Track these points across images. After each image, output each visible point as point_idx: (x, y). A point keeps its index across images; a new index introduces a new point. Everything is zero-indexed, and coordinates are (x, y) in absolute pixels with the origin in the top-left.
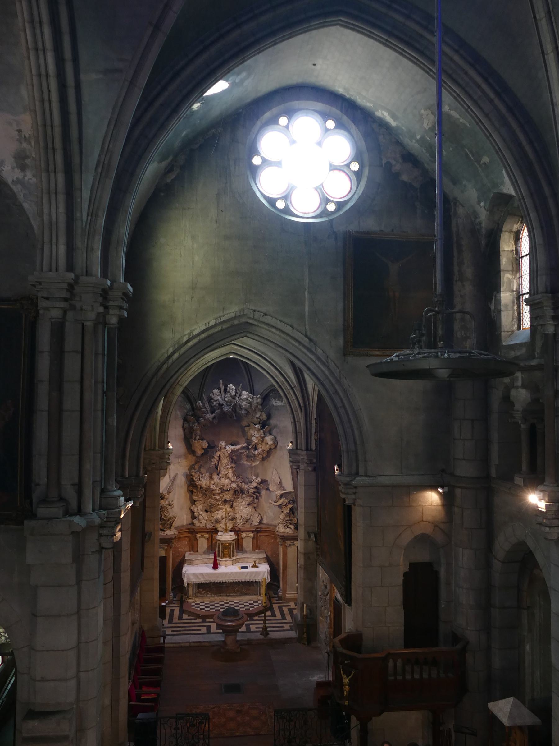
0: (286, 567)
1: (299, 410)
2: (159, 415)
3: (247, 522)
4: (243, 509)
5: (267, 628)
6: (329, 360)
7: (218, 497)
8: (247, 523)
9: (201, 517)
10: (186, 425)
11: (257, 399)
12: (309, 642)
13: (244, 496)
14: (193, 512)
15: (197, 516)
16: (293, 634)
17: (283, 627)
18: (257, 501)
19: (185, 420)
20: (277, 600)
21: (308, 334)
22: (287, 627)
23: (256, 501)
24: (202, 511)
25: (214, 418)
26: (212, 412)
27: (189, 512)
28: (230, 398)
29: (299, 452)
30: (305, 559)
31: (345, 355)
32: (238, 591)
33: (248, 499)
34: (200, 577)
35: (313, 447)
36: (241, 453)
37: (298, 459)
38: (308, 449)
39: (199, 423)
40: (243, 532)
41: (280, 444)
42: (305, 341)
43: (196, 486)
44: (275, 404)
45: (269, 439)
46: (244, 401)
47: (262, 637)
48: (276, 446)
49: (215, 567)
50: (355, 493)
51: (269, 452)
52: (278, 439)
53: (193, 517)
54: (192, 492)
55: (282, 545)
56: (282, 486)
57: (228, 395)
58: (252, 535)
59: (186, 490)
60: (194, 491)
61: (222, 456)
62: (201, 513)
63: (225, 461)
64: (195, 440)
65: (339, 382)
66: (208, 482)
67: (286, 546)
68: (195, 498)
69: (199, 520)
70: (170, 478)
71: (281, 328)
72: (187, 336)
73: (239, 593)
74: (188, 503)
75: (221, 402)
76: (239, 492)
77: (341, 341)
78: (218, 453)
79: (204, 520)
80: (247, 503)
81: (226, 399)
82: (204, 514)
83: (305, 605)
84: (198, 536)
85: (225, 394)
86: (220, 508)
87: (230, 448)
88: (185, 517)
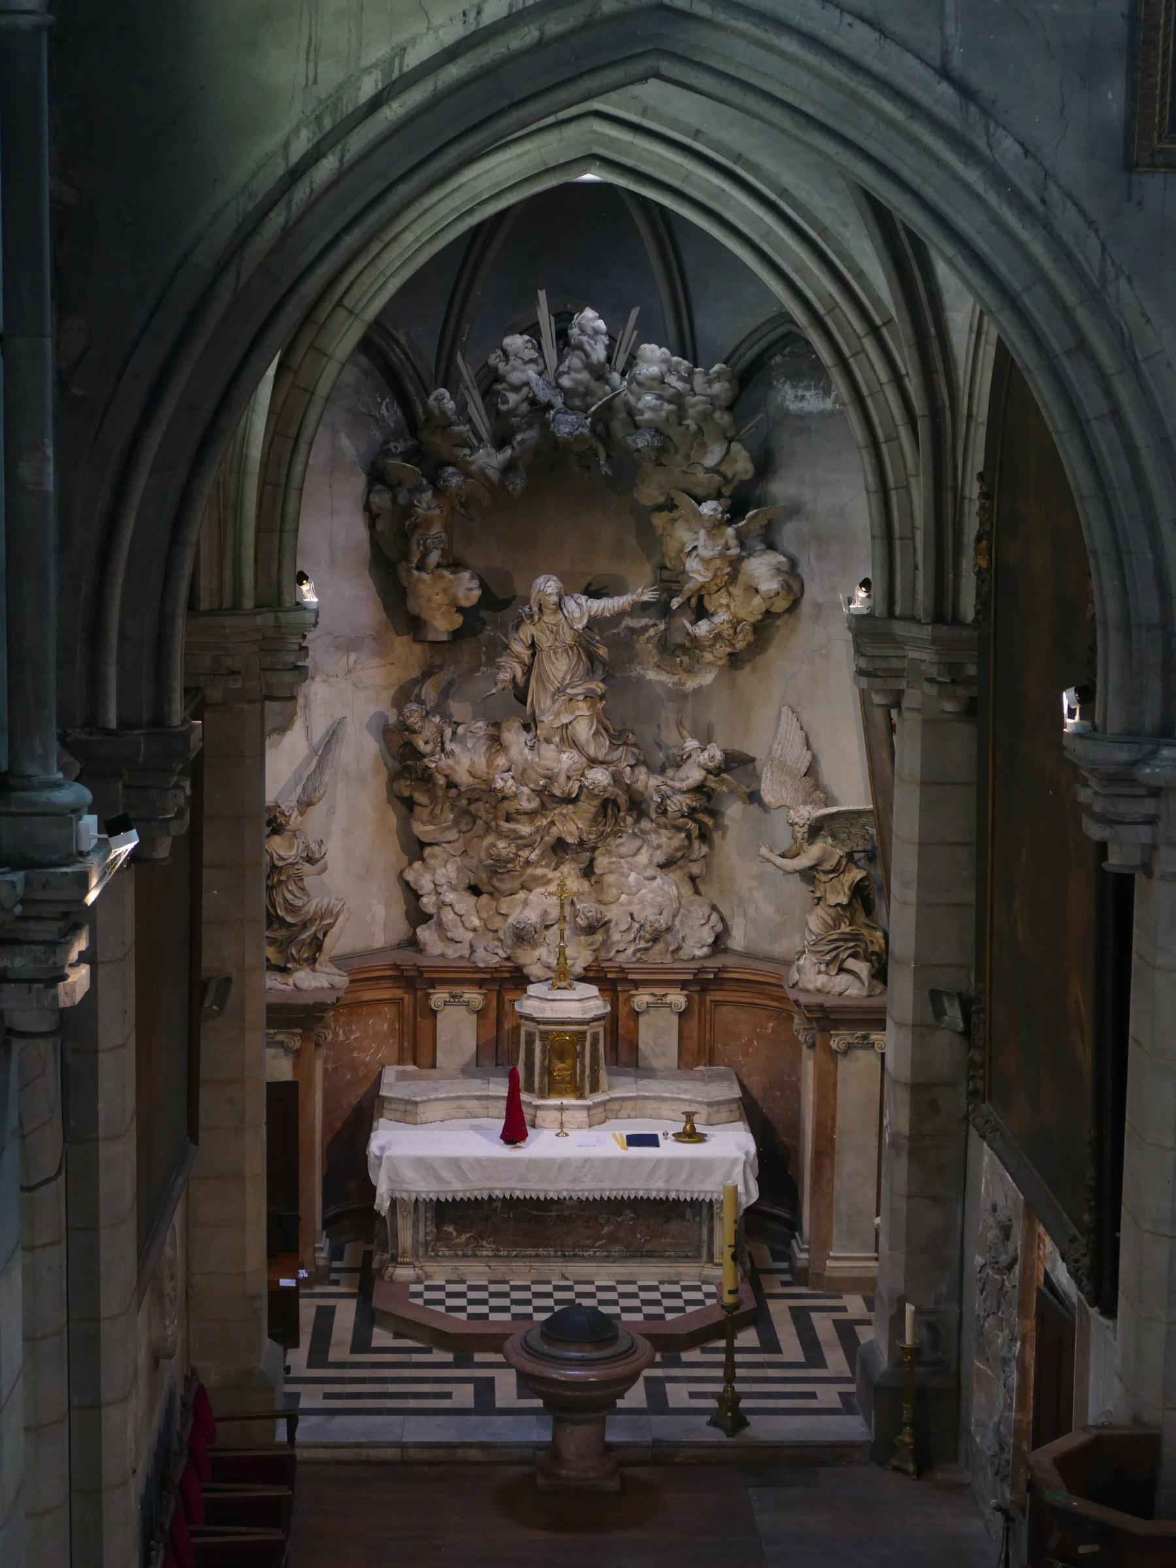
1: (904, 433)
2: (256, 452)
4: (639, 886)
5: (738, 1397)
6: (1054, 192)
7: (525, 829)
8: (659, 946)
9: (448, 916)
10: (381, 500)
11: (710, 383)
12: (924, 1464)
13: (645, 824)
14: (412, 894)
15: (431, 909)
16: (854, 1428)
17: (813, 1395)
18: (705, 849)
19: (377, 476)
20: (785, 1284)
21: (957, 62)
22: (828, 1396)
24: (454, 888)
27: (398, 893)
28: (584, 376)
29: (899, 628)
30: (915, 1106)
31: (1130, 166)
32: (613, 1239)
34: (446, 1174)
35: (968, 608)
36: (632, 631)
37: (896, 664)
38: (942, 613)
39: (438, 492)
40: (637, 984)
41: (813, 592)
42: (941, 97)
43: (426, 778)
44: (793, 406)
46: (649, 389)
47: (717, 1436)
49: (514, 1133)
50: (1152, 821)
52: (803, 570)
54: (408, 805)
55: (812, 1046)
56: (818, 786)
57: (574, 360)
58: (677, 998)
60: (420, 797)
61: (545, 641)
62: (450, 897)
64: (421, 567)
65: (1095, 297)
66: (481, 762)
67: (833, 1054)
68: (422, 829)
69: (440, 926)
70: (308, 737)
71: (823, 33)
72: (377, 74)
73: (617, 1249)
74: (390, 854)
75: (544, 395)
76: (620, 808)
77: (1113, 97)
78: (527, 632)
79: (463, 929)
80: (660, 857)
81: (566, 381)
83: (910, 1308)
84: (439, 996)
87: (582, 609)
88: (380, 911)
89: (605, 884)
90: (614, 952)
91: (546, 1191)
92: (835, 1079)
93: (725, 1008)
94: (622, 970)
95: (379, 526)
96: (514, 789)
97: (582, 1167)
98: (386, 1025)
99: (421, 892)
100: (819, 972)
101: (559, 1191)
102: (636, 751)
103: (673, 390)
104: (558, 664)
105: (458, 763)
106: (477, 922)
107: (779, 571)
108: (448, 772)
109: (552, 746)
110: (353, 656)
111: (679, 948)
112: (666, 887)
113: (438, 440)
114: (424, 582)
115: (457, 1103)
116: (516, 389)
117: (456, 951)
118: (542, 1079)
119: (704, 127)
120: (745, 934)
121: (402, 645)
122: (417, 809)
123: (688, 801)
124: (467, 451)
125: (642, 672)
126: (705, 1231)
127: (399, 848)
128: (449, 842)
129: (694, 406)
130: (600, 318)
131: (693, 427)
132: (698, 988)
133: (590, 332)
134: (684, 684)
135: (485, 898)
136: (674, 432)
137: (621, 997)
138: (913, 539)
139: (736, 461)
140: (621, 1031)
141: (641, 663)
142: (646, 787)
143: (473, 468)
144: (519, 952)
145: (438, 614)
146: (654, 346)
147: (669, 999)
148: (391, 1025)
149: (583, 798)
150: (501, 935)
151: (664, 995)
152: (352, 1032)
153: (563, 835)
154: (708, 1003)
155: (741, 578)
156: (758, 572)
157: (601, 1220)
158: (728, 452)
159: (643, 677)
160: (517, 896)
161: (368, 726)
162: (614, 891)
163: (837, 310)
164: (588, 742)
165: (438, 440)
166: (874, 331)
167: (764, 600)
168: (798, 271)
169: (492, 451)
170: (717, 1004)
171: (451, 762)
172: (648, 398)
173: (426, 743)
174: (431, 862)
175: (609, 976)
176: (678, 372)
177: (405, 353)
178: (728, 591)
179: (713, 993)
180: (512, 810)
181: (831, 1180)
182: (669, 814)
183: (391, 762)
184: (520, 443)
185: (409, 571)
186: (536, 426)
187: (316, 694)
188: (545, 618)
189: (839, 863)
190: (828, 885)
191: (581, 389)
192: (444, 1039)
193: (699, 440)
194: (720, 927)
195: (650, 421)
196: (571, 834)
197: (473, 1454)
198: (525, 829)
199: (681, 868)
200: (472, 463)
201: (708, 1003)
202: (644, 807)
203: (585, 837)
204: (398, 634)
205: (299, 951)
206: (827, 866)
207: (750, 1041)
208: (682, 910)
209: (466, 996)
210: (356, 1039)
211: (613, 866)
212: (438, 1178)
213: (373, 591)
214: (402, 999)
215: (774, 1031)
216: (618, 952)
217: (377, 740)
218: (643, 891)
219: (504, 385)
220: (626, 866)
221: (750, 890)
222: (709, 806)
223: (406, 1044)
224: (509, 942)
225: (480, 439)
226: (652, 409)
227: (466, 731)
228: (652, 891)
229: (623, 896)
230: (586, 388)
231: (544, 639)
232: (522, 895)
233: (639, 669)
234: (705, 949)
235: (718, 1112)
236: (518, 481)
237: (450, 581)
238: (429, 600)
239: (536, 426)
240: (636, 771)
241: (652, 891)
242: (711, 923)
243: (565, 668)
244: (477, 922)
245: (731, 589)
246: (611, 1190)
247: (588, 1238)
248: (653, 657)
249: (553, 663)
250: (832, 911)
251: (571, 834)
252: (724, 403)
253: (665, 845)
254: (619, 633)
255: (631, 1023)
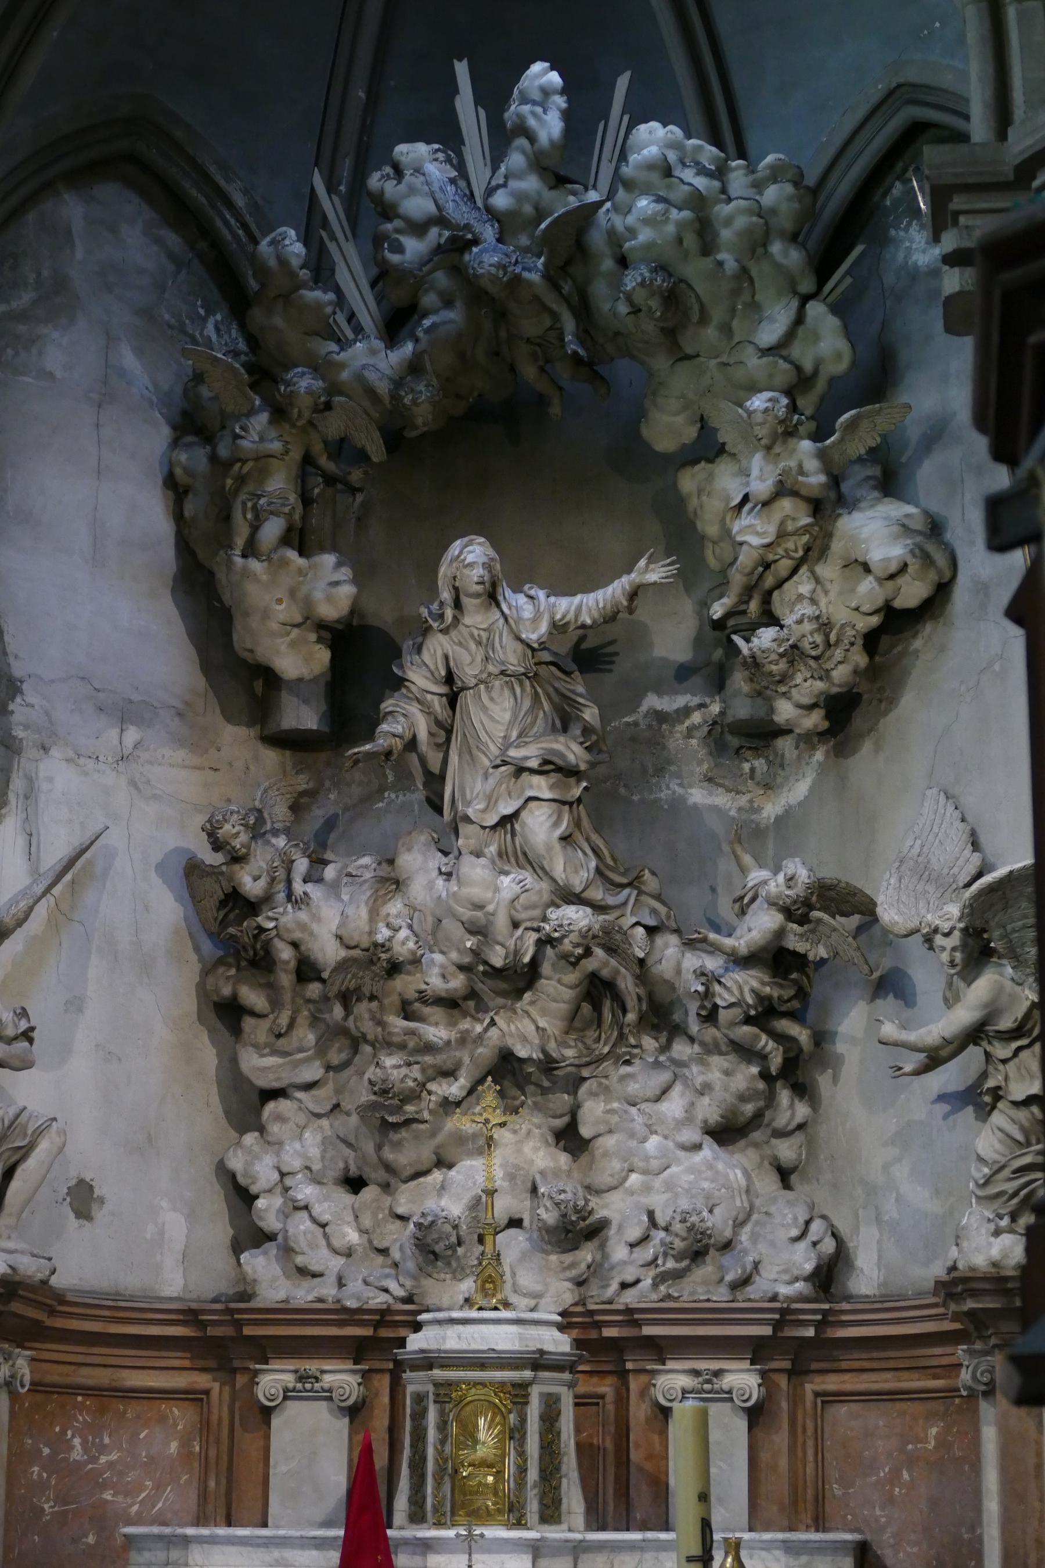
3: (697, 1254)
4: (661, 1150)
7: (436, 1032)
8: (706, 1271)
9: (301, 1226)
10: (194, 458)
11: (759, 186)
13: (681, 1049)
14: (242, 1196)
15: (271, 1222)
18: (802, 1111)
23: (790, 1109)
24: (317, 1180)
25: (414, 367)
26: (396, 324)
27: (215, 1200)
28: (531, 184)
33: (715, 1076)
36: (661, 717)
39: (279, 413)
43: (258, 961)
48: (943, 591)
51: (894, 628)
53: (250, 1236)
54: (229, 1015)
58: (743, 1379)
59: (190, 1004)
60: (253, 997)
61: (469, 670)
62: (305, 1192)
63: (496, 716)
64: (250, 550)
68: (260, 1065)
69: (288, 1251)
70: (31, 852)
74: (202, 1114)
78: (437, 646)
79: (332, 1247)
80: (709, 1110)
81: (501, 201)
82: (331, 1204)
84: (274, 1379)
85: (496, 159)
86: (460, 1139)
87: (537, 611)
88: (176, 1226)
89: (598, 1153)
90: (614, 1286)
94: (631, 1316)
95: (189, 509)
96: (411, 945)
98: (174, 1446)
99: (254, 1189)
100: (997, 1233)
102: (662, 909)
103: (686, 188)
104: (495, 710)
105: (316, 918)
106: (353, 1237)
107: (906, 529)
108: (297, 935)
109: (483, 861)
110: (132, 735)
111: (745, 1281)
112: (720, 1166)
114: (257, 580)
116: (419, 229)
117: (308, 1292)
120: (880, 1257)
121: (236, 740)
123: (755, 984)
124: (333, 347)
125: (679, 790)
127: (220, 1111)
128: (309, 1087)
129: (728, 221)
130: (552, 69)
132: (787, 1365)
133: (536, 95)
134: (759, 810)
135: (369, 1193)
139: (816, 337)
140: (635, 1456)
141: (678, 775)
142: (678, 971)
143: (345, 375)
144: (427, 1283)
146: (654, 125)
147: (729, 1381)
149: (546, 968)
150: (396, 1255)
152: (103, 1449)
153: (510, 1042)
154: (809, 1397)
155: (837, 546)
156: (865, 532)
158: (799, 320)
159: (683, 799)
160: (429, 1179)
161: (161, 868)
164: (549, 848)
165: (278, 321)
167: (880, 581)
169: (379, 344)
170: (828, 1399)
171: (303, 916)
172: (643, 203)
173: (256, 879)
174: (274, 1128)
175: (609, 1332)
176: (697, 163)
177: (244, 226)
178: (813, 572)
179: (818, 1379)
180: (411, 995)
182: (723, 1015)
184: (427, 331)
185: (229, 562)
186: (459, 304)
187: (50, 779)
188: (467, 620)
189: (1028, 1016)
190: (1011, 1066)
191: (528, 209)
192: (283, 1468)
193: (746, 297)
194: (829, 1246)
195: (650, 246)
196: (524, 1039)
198: (436, 1032)
199: (756, 1145)
200: (342, 366)
201: (809, 1397)
202: (677, 1017)
204: (229, 719)
206: (1006, 1023)
207: (895, 1473)
208: (755, 1217)
209: (328, 1378)
210: (111, 1465)
211: (615, 1119)
213: (179, 629)
214: (207, 1392)
215: (942, 1442)
216: (624, 1286)
217: (179, 899)
218: (674, 1169)
219: (398, 223)
220: (640, 1120)
221: (886, 1168)
222: (760, 899)
223: (212, 1484)
224: (410, 1265)
225: (358, 330)
226: (648, 221)
227: (340, 872)
228: (691, 1170)
229: (634, 1177)
230: (537, 208)
232: (437, 1176)
233: (674, 786)
234: (799, 1286)
236: (421, 387)
237: (300, 572)
238: (266, 615)
239: (459, 304)
240: (660, 940)
241: (691, 1170)
242: (812, 1237)
243: (507, 716)
244: (353, 1237)
245: (819, 569)
248: (700, 763)
249: (485, 709)
250: (1022, 1115)
251: (524, 1039)
252: (788, 225)
253: (718, 1086)
254: (636, 724)
255: (656, 1438)
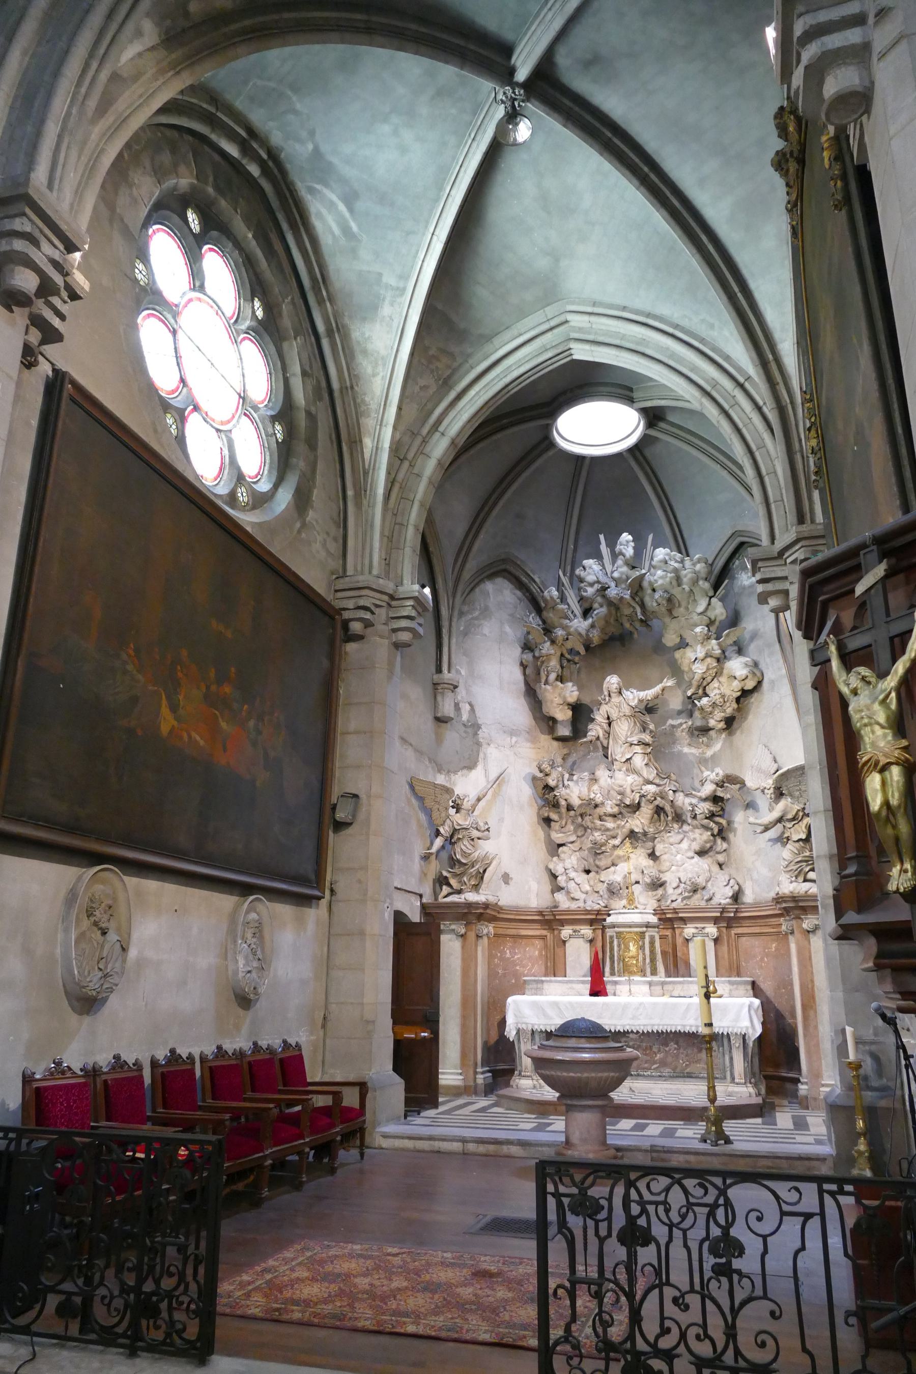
0: (813, 998)
1: (766, 436)
2: (380, 490)
4: (680, 857)
8: (697, 896)
9: (572, 885)
10: (528, 657)
11: (694, 565)
13: (686, 828)
15: (563, 884)
18: (725, 845)
19: (527, 647)
23: (721, 845)
25: (593, 626)
27: (546, 878)
32: (663, 1063)
33: (697, 836)
34: (550, 1012)
36: (673, 726)
40: (684, 920)
45: (737, 666)
46: (660, 568)
48: (760, 683)
49: (598, 989)
52: (762, 666)
54: (547, 821)
57: (620, 562)
58: (712, 930)
59: (535, 819)
60: (554, 816)
61: (614, 715)
62: (572, 874)
63: (623, 728)
64: (546, 683)
66: (585, 791)
69: (568, 893)
73: (667, 1071)
74: (539, 852)
75: (603, 579)
76: (666, 814)
78: (604, 709)
79: (582, 893)
80: (696, 846)
81: (616, 575)
82: (581, 878)
86: (619, 857)
88: (534, 886)
90: (669, 901)
91: (615, 1025)
92: (810, 952)
93: (744, 939)
94: (675, 911)
97: (638, 1009)
98: (537, 953)
100: (791, 882)
101: (624, 1026)
104: (623, 727)
105: (572, 791)
106: (588, 888)
108: (566, 797)
110: (514, 739)
111: (711, 899)
113: (551, 615)
115: (570, 985)
116: (591, 585)
118: (619, 964)
119: (627, 304)
122: (553, 824)
126: (727, 1058)
128: (572, 842)
129: (686, 576)
131: (687, 588)
136: (676, 591)
137: (677, 931)
138: (775, 472)
139: (715, 609)
140: (679, 954)
143: (572, 629)
145: (557, 710)
146: (661, 549)
147: (706, 931)
148: (540, 953)
149: (643, 804)
151: (703, 928)
152: (516, 954)
155: (725, 671)
157: (655, 1049)
158: (709, 604)
159: (681, 751)
161: (525, 778)
162: (668, 864)
163: (718, 386)
165: (551, 615)
166: (741, 386)
168: (692, 370)
169: (581, 620)
170: (739, 935)
171: (568, 791)
174: (562, 856)
180: (602, 814)
181: (816, 1027)
183: (539, 801)
189: (797, 814)
193: (692, 598)
194: (736, 888)
195: (662, 585)
197: (515, 1150)
200: (571, 627)
202: (684, 818)
203: (646, 828)
204: (542, 733)
205: (469, 880)
206: (790, 816)
207: (762, 959)
212: (545, 1015)
218: (686, 865)
224: (606, 896)
225: (575, 616)
226: (661, 577)
228: (691, 865)
231: (613, 711)
232: (612, 868)
233: (679, 747)
235: (737, 989)
237: (562, 688)
238: (552, 701)
240: (677, 794)
241: (691, 865)
242: (731, 884)
244: (588, 888)
245: (720, 679)
246: (659, 1025)
247: (646, 1062)
250: (797, 845)
251: (637, 826)
252: (704, 576)
